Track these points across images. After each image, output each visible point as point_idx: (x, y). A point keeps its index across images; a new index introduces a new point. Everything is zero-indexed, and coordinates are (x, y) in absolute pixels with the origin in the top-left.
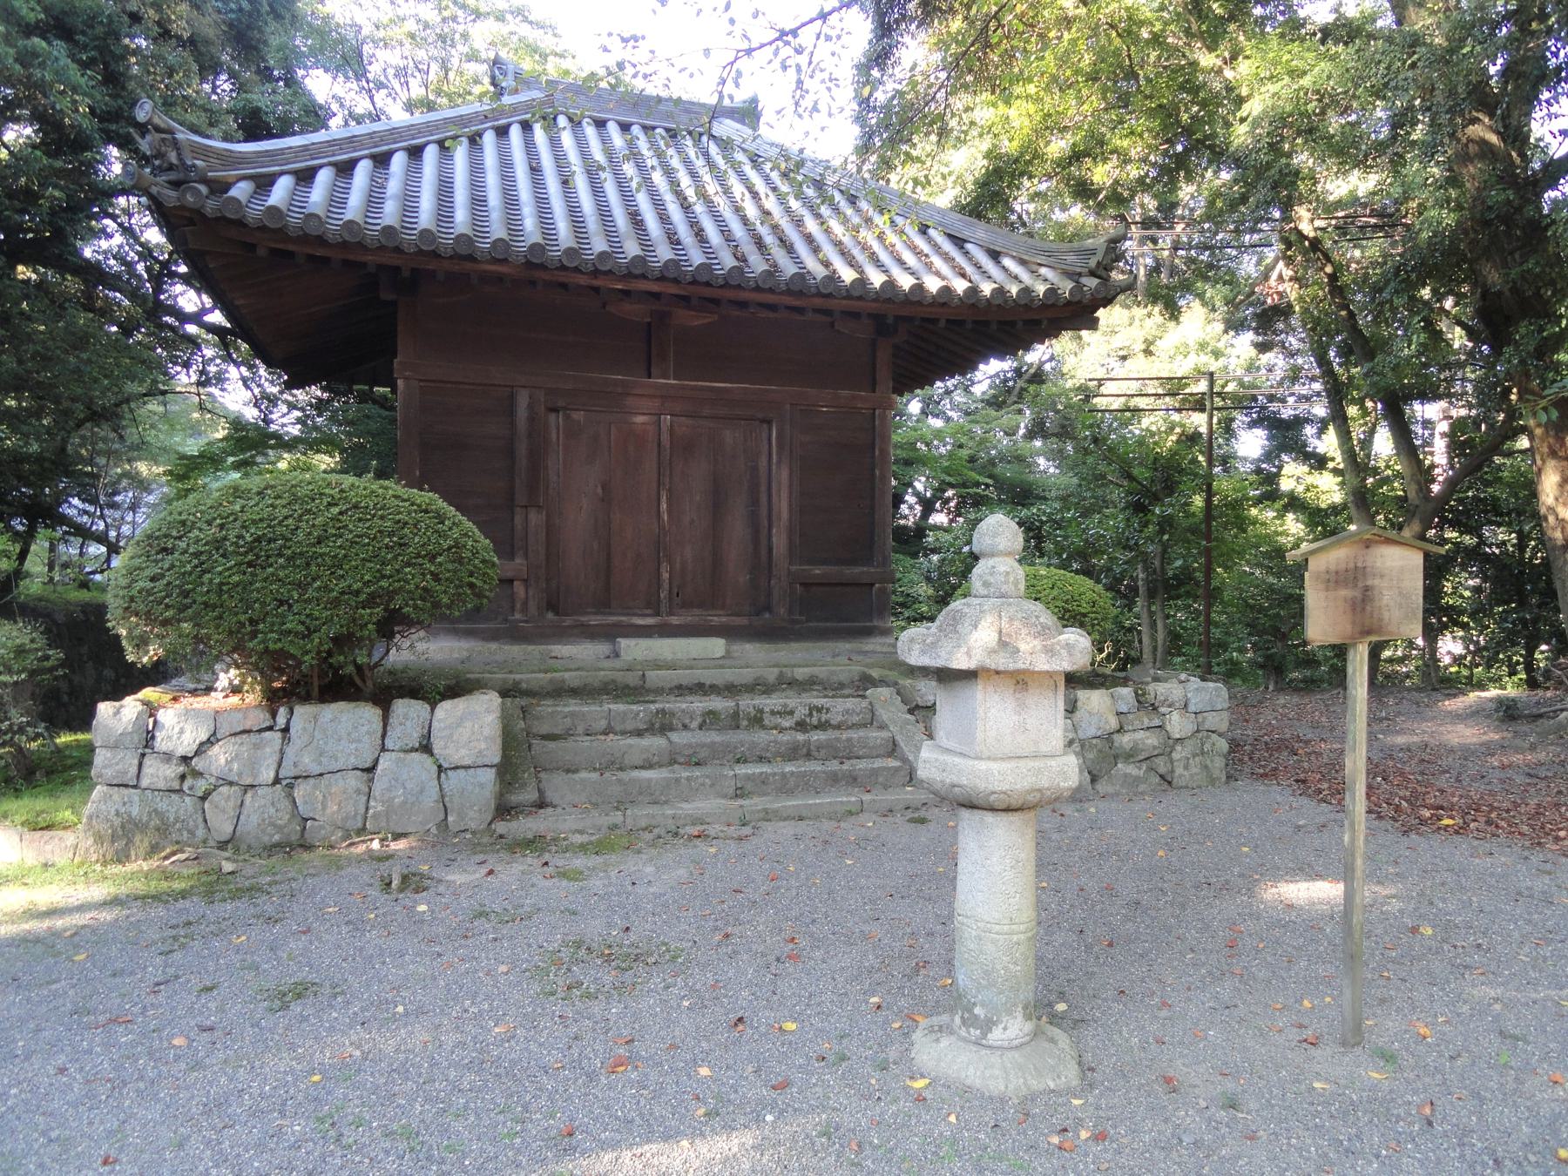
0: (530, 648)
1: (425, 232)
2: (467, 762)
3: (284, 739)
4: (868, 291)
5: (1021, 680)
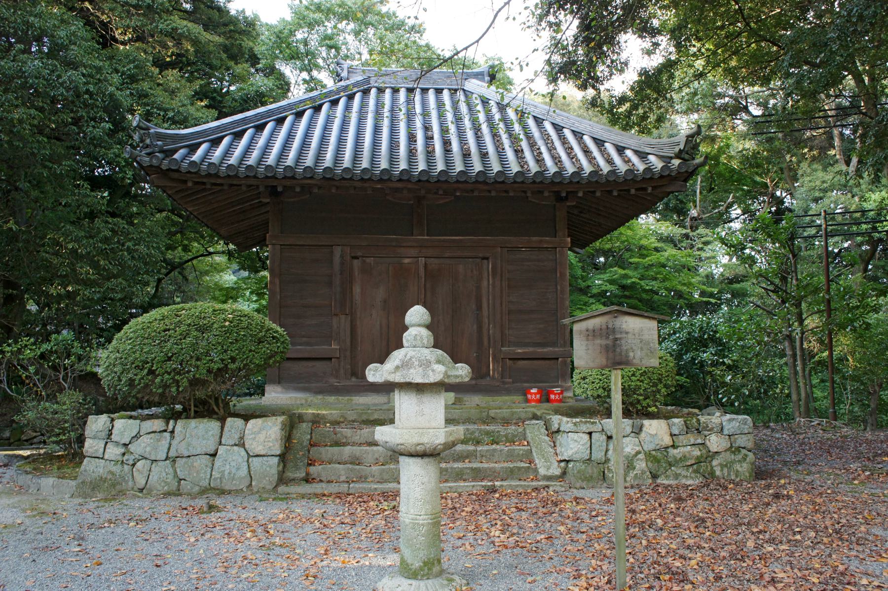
0: (340, 398)
2: (262, 453)
4: (507, 178)
5: (419, 388)
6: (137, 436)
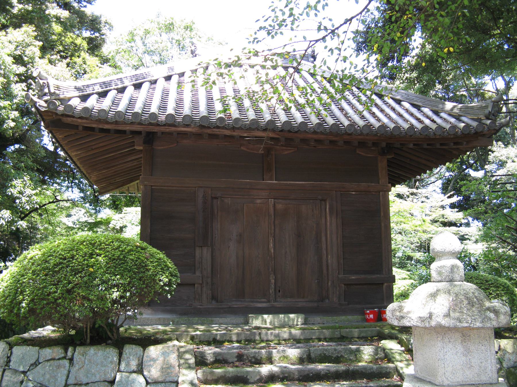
1: (153, 114)
3: (70, 363)
6: (36, 364)
